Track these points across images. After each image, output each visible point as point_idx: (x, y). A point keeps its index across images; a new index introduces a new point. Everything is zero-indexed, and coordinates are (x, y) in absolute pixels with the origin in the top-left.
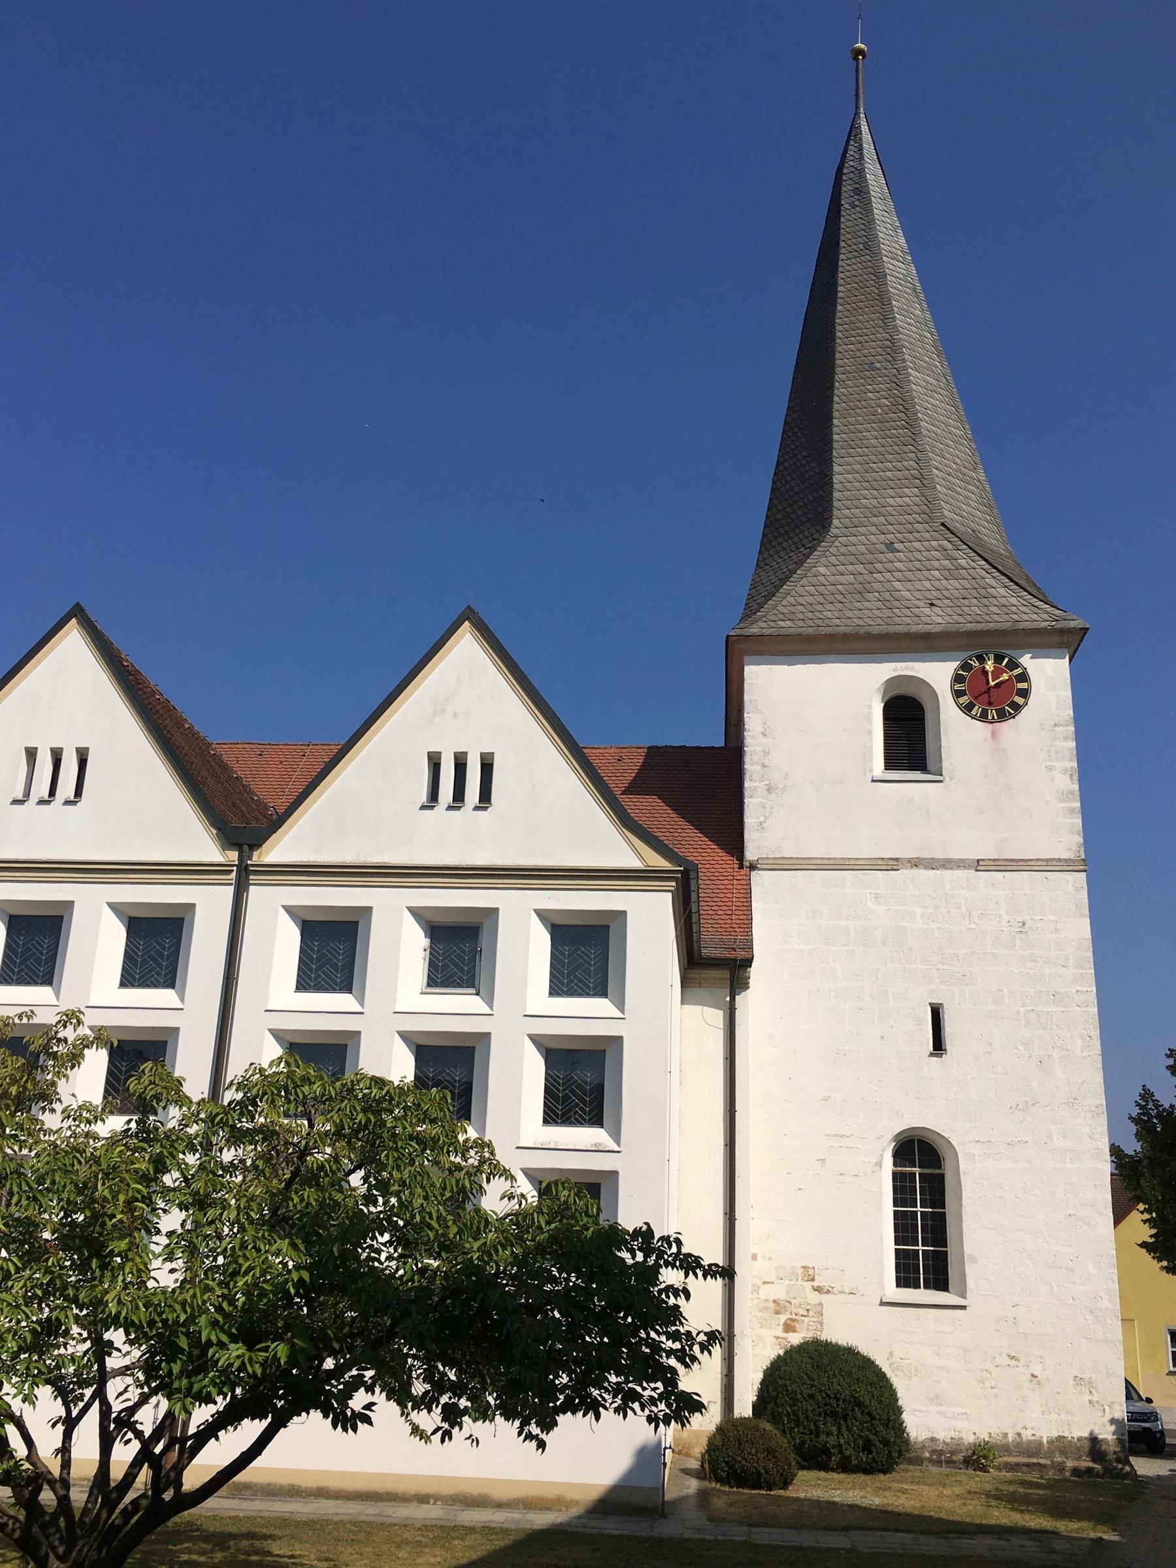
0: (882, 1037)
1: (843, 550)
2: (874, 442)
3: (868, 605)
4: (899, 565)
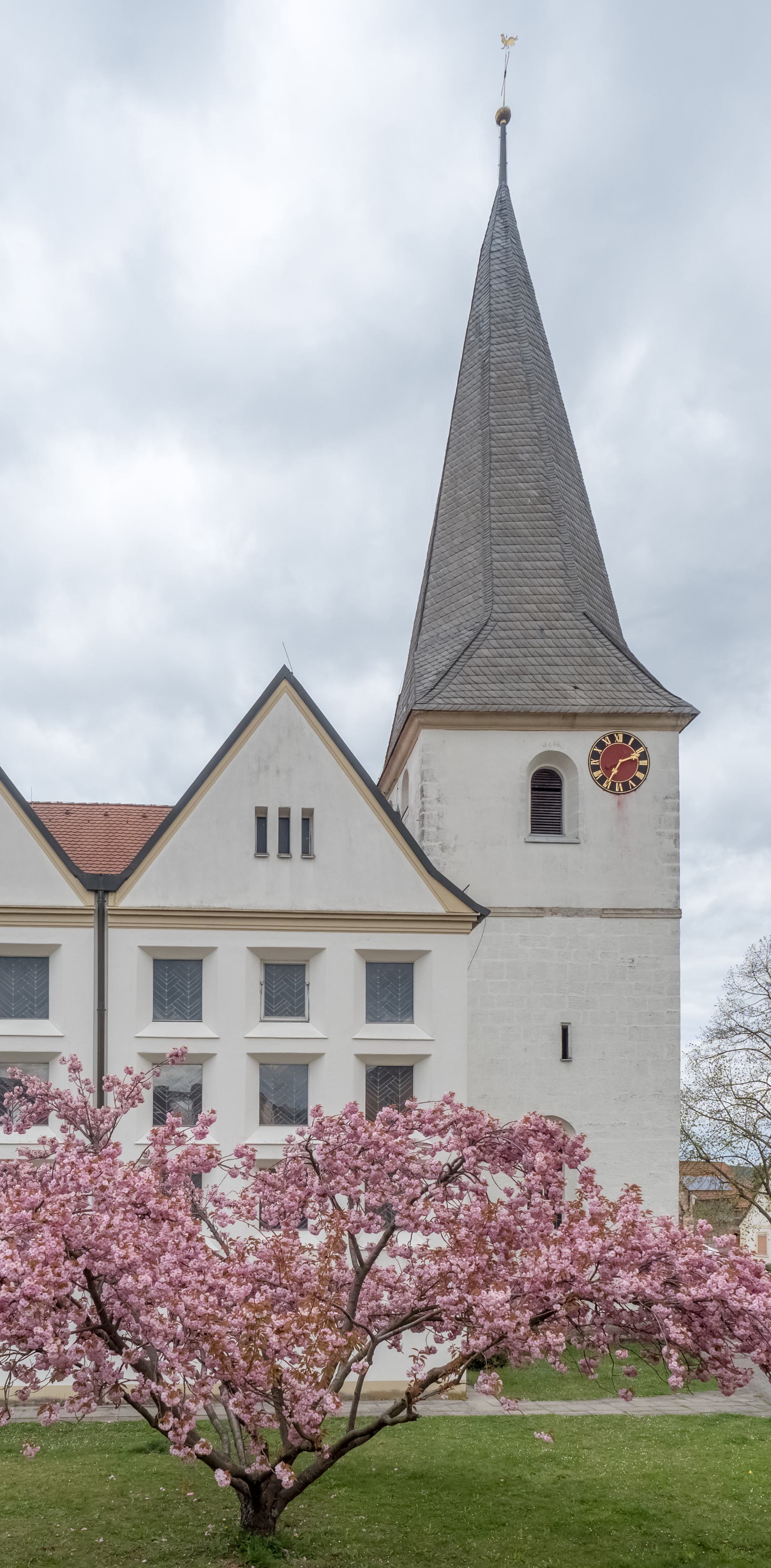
0: (525, 1050)
1: (502, 634)
2: (526, 531)
3: (524, 686)
4: (549, 651)
